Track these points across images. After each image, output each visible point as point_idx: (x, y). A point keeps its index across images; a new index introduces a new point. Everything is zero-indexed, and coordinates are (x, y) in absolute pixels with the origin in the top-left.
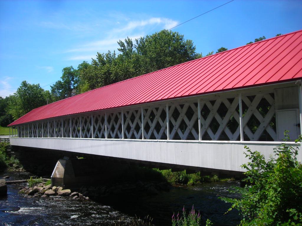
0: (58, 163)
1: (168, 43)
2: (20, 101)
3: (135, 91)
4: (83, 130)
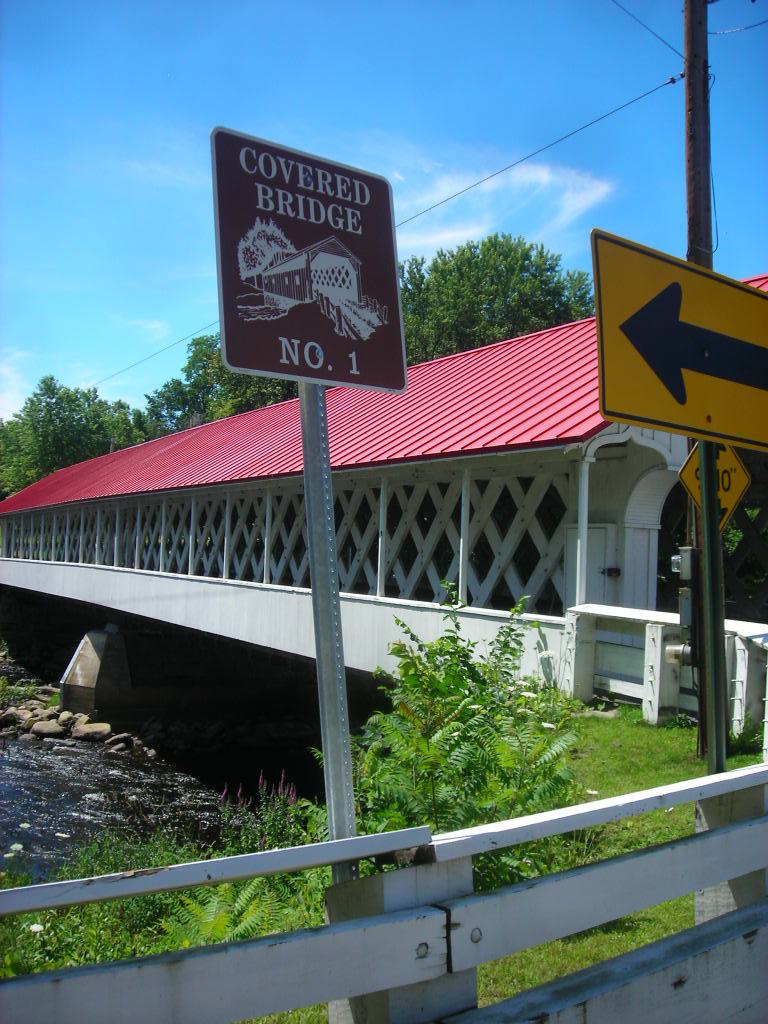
0: (86, 638)
1: (502, 280)
2: (30, 439)
3: (376, 435)
4: (278, 549)
